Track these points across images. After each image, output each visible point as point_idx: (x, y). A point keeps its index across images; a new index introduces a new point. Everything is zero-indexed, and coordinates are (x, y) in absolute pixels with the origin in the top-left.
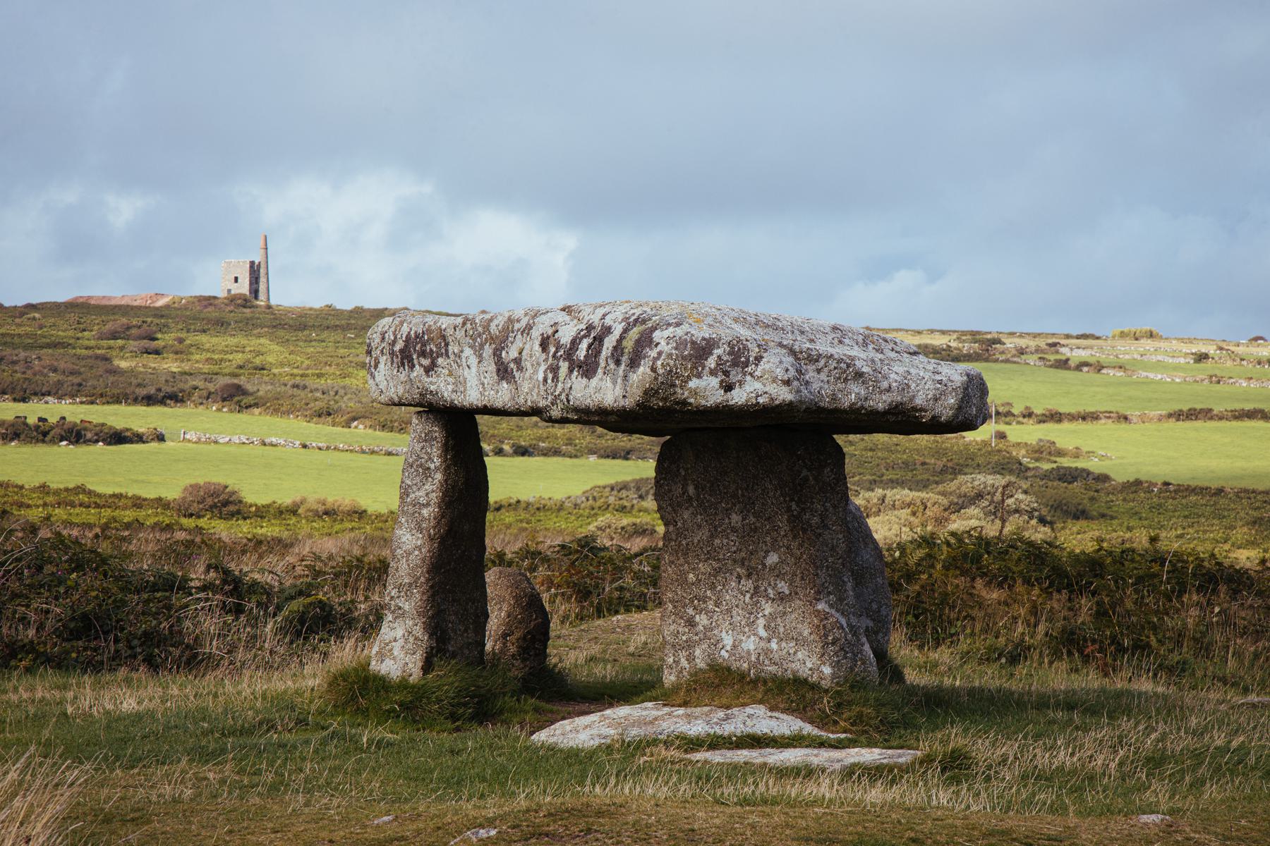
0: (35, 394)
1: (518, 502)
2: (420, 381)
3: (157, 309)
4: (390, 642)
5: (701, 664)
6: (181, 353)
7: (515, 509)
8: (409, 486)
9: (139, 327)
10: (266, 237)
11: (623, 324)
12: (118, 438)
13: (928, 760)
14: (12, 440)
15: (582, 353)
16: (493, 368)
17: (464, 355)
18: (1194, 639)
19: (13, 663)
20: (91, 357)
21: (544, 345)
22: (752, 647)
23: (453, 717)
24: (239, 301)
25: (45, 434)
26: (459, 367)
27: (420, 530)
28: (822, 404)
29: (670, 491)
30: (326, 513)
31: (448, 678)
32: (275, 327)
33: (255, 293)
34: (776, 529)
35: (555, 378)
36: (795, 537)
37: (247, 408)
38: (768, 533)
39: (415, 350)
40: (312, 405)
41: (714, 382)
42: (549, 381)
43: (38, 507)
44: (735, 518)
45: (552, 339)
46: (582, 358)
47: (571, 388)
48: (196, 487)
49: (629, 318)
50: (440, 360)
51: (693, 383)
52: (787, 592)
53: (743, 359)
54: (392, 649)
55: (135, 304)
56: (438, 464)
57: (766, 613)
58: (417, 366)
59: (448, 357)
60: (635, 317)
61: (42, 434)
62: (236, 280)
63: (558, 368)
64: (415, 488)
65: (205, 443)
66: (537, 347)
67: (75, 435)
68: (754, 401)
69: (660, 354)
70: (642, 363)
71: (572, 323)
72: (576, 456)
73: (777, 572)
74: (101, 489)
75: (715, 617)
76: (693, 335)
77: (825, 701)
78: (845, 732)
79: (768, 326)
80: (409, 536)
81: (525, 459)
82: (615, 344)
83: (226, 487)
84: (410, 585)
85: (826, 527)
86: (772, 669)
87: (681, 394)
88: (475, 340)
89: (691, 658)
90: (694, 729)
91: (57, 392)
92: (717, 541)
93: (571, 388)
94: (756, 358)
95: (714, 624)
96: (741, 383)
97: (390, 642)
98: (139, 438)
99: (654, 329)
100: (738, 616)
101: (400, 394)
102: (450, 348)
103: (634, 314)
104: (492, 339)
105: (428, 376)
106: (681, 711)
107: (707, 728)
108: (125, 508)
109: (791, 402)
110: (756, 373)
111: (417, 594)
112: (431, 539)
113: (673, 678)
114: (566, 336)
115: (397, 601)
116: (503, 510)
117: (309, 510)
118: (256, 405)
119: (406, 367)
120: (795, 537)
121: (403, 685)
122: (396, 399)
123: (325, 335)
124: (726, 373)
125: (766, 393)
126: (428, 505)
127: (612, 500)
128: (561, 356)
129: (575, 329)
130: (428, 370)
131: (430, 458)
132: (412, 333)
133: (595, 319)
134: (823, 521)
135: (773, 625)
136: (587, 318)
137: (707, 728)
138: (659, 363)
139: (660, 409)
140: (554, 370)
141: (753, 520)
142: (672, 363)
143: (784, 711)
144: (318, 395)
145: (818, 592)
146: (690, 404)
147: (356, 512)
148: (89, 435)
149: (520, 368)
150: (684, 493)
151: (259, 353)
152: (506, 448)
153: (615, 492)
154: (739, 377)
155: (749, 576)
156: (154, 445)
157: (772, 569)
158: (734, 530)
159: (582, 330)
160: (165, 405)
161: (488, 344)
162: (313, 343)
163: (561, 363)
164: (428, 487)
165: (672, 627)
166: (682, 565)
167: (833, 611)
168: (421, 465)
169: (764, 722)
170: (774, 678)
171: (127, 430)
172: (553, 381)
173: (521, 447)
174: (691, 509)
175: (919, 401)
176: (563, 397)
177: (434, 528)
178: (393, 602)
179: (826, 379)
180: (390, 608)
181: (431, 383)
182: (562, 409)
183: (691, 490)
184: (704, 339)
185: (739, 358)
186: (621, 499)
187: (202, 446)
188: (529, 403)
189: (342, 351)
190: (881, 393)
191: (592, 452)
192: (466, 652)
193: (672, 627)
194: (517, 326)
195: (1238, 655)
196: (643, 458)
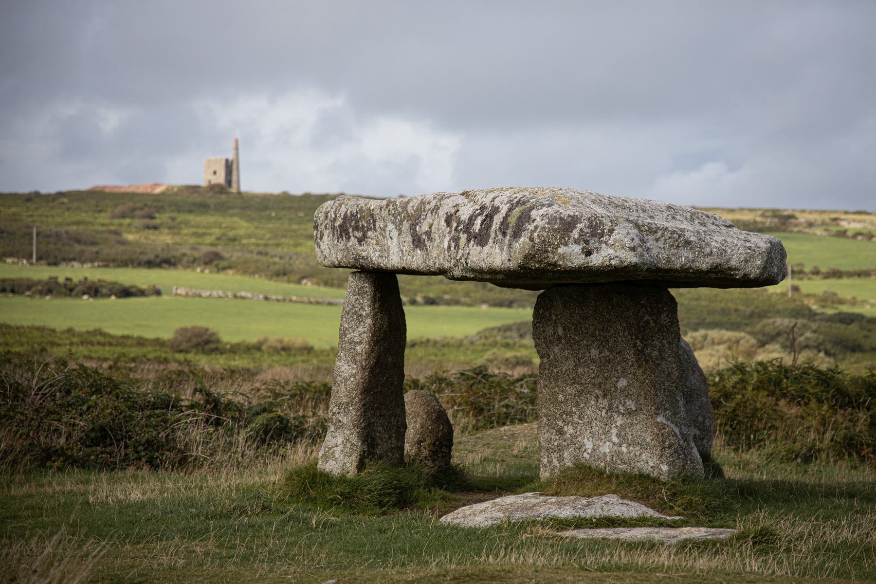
0: (64, 260)
4: (333, 447)
5: (569, 464)
8: (346, 328)
10: (237, 142)
11: (508, 205)
12: (126, 293)
14: (47, 294)
16: (409, 239)
17: (388, 229)
19: (48, 464)
21: (448, 221)
22: (607, 450)
23: (381, 504)
27: (355, 362)
28: (660, 265)
30: (283, 349)
33: (229, 182)
34: (625, 360)
35: (457, 246)
36: (639, 366)
39: (350, 225)
41: (578, 249)
42: (452, 249)
44: (594, 352)
45: (454, 217)
47: (469, 254)
48: (184, 330)
49: (513, 200)
51: (562, 250)
52: (634, 408)
53: (599, 231)
54: (334, 453)
56: (368, 312)
57: (618, 424)
58: (352, 238)
59: (376, 231)
60: (517, 200)
62: (215, 173)
63: (459, 238)
64: (351, 330)
66: (443, 223)
67: (95, 290)
69: (536, 227)
70: (523, 234)
73: (626, 393)
76: (561, 213)
77: (663, 492)
78: (679, 515)
79: (618, 206)
80: (346, 366)
82: (502, 220)
83: (207, 330)
84: (348, 403)
85: (663, 358)
87: (552, 258)
88: (396, 218)
89: (561, 459)
91: (81, 259)
92: (580, 370)
93: (469, 254)
94: (609, 231)
95: (578, 433)
96: (598, 249)
97: (333, 447)
98: (142, 293)
100: (597, 427)
101: (339, 259)
102: (377, 224)
103: (516, 198)
104: (409, 217)
105: (361, 245)
108: (131, 346)
109: (636, 265)
110: (610, 242)
114: (465, 214)
115: (338, 416)
116: (417, 347)
117: (270, 347)
118: (230, 267)
119: (344, 239)
120: (639, 366)
121: (342, 480)
124: (587, 242)
125: (617, 257)
126: (360, 343)
129: (472, 209)
130: (360, 241)
131: (362, 308)
132: (348, 212)
133: (487, 201)
134: (661, 354)
135: (623, 433)
136: (480, 201)
137: (573, 512)
138: (536, 234)
139: (537, 270)
140: (456, 240)
142: (545, 234)
145: (658, 409)
146: (559, 265)
149: (430, 239)
150: (555, 334)
152: (419, 299)
155: (605, 396)
156: (153, 298)
157: (622, 391)
158: (593, 361)
159: (477, 210)
163: (461, 235)
165: (546, 436)
166: (553, 388)
167: (669, 423)
168: (355, 313)
170: (625, 474)
172: (455, 248)
174: (561, 345)
175: (733, 263)
176: (463, 260)
178: (334, 417)
179: (662, 246)
180: (332, 421)
181: (363, 250)
183: (560, 331)
184: (569, 216)
188: (437, 265)
190: (704, 256)
191: (484, 302)
192: (390, 454)
193: (546, 436)
194: (428, 207)
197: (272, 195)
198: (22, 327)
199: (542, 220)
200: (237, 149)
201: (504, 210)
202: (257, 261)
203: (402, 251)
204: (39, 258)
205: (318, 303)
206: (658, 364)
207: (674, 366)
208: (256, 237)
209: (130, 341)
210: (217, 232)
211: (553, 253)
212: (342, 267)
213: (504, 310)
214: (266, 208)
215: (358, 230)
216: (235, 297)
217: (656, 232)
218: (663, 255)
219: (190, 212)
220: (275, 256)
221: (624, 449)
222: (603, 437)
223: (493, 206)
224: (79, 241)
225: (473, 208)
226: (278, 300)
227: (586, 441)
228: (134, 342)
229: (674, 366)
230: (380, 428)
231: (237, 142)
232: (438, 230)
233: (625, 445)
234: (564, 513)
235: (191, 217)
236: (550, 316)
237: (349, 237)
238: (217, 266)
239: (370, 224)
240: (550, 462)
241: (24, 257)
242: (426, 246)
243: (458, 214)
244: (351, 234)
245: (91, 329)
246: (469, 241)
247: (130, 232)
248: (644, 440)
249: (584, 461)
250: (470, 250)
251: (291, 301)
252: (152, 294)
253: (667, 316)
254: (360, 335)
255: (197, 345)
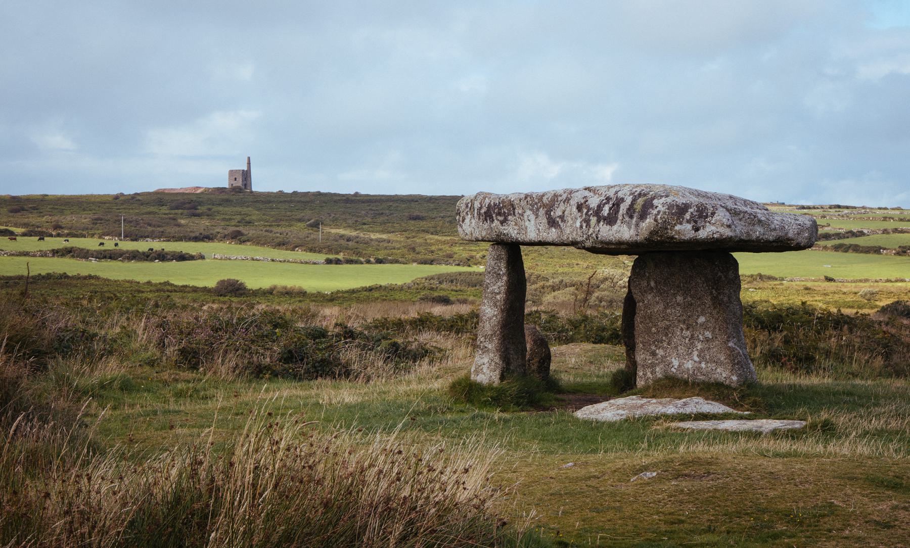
0: (142, 237)
1: (381, 286)
2: (497, 228)
3: (197, 194)
5: (659, 375)
6: (211, 215)
7: (379, 290)
9: (190, 203)
10: (249, 158)
11: (632, 196)
13: (813, 426)
14: (132, 259)
15: (606, 211)
16: (545, 221)
17: (526, 215)
18: (835, 353)
19: (261, 375)
20: (167, 218)
21: (579, 207)
22: (690, 366)
23: (518, 404)
24: (237, 190)
25: (148, 256)
26: (522, 220)
27: (495, 306)
28: (742, 237)
29: (640, 284)
30: (287, 293)
31: (512, 386)
32: (255, 202)
34: (704, 304)
35: (588, 225)
36: (715, 308)
37: (244, 242)
38: (699, 306)
39: (494, 212)
40: (275, 240)
41: (689, 227)
42: (584, 227)
43: (147, 292)
44: (679, 299)
45: (584, 205)
46: (606, 215)
47: (599, 231)
48: (223, 282)
49: (634, 193)
50: (510, 217)
51: (678, 227)
52: (711, 337)
53: (704, 214)
55: (187, 192)
58: (496, 221)
59: (515, 216)
60: (638, 193)
61: (148, 256)
62: (236, 179)
63: (590, 220)
64: (492, 284)
65: (225, 259)
66: (574, 209)
67: (162, 256)
68: (711, 236)
69: (659, 212)
70: (648, 217)
71: (595, 197)
72: (406, 263)
73: (704, 327)
74: (176, 283)
75: (668, 351)
76: (677, 202)
77: (735, 394)
78: (748, 411)
79: (704, 196)
80: (489, 309)
81: (381, 265)
82: (628, 207)
83: (238, 281)
84: (492, 335)
85: (731, 302)
86: (702, 377)
87: (671, 233)
88: (533, 206)
89: (653, 373)
90: (670, 410)
91: (152, 236)
92: (668, 311)
93: (599, 231)
94: (712, 214)
98: (192, 258)
99: (653, 198)
100: (681, 349)
101: (483, 235)
102: (516, 211)
103: (636, 191)
104: (544, 206)
105: (503, 226)
106: (654, 401)
107: (676, 410)
108: (189, 292)
109: (731, 237)
111: (496, 340)
112: (502, 311)
113: (643, 383)
114: (594, 202)
115: (484, 344)
116: (373, 291)
117: (278, 292)
118: (248, 241)
119: (488, 221)
120: (715, 308)
121: (490, 387)
122: (480, 238)
123: (279, 206)
124: (696, 222)
125: (718, 232)
126: (499, 293)
127: (426, 284)
128: (591, 214)
129: (598, 200)
130: (502, 223)
132: (492, 203)
133: (611, 193)
134: (729, 300)
135: (702, 355)
136: (604, 194)
137: (676, 410)
138: (659, 217)
140: (587, 222)
141: (690, 299)
142: (666, 216)
143: (713, 400)
144: (278, 235)
145: (729, 337)
146: (676, 238)
147: (301, 293)
148: (169, 257)
149: (563, 221)
151: (247, 215)
152: (372, 259)
153: (428, 281)
154: (703, 224)
155: (687, 329)
156: (200, 261)
157: (702, 325)
158: (678, 304)
159: (603, 200)
160: (204, 241)
161: (541, 209)
162: (274, 210)
163: (591, 218)
164: (499, 284)
165: (642, 356)
166: (648, 323)
167: (736, 347)
168: (495, 273)
169: (705, 406)
170: (704, 382)
171: (187, 254)
172: (586, 227)
173: (378, 259)
174: (653, 294)
175: (790, 235)
176: (594, 235)
177: (504, 305)
178: (482, 344)
179: (744, 224)
180: (480, 348)
181: (504, 229)
182: (592, 242)
183: (652, 284)
184: (683, 204)
185: (702, 214)
186: (431, 284)
187: (223, 261)
188: (571, 239)
189: (288, 213)
190: (771, 231)
191: (414, 261)
192: (518, 369)
193: (642, 356)
194: (560, 198)
195: (858, 361)
196: (440, 264)
197: (272, 193)
198: (119, 281)
199: (663, 207)
200: (249, 163)
201: (629, 200)
202: (266, 236)
203: (539, 230)
204: (126, 236)
205: (306, 263)
206: (728, 306)
207: (738, 307)
208: (262, 220)
209: (188, 289)
210: (239, 218)
211: (671, 230)
212: (485, 241)
213: (427, 267)
214: (270, 202)
215: (500, 216)
216: (253, 259)
217: (739, 214)
218: (745, 230)
219: (220, 205)
220: (277, 233)
221: (703, 365)
222: (687, 357)
223: (617, 197)
224: (150, 225)
225: (600, 198)
226: (280, 261)
227: (673, 360)
228: (191, 290)
229: (738, 307)
230: (512, 352)
231: (249, 158)
232: (571, 214)
233: (704, 363)
234: (670, 410)
235: (221, 208)
236: (645, 273)
237: (493, 220)
238: (239, 240)
239: (510, 211)
240: (645, 375)
241: (116, 236)
242: (560, 226)
243: (587, 203)
244: (494, 218)
245: (162, 281)
246: (598, 221)
247: (181, 219)
248: (719, 359)
249: (672, 373)
250: (600, 228)
251: (288, 261)
252: (199, 258)
253: (733, 273)
254: (499, 288)
255: (231, 292)
